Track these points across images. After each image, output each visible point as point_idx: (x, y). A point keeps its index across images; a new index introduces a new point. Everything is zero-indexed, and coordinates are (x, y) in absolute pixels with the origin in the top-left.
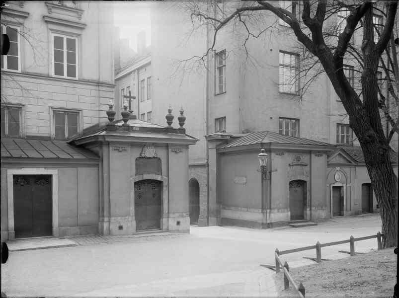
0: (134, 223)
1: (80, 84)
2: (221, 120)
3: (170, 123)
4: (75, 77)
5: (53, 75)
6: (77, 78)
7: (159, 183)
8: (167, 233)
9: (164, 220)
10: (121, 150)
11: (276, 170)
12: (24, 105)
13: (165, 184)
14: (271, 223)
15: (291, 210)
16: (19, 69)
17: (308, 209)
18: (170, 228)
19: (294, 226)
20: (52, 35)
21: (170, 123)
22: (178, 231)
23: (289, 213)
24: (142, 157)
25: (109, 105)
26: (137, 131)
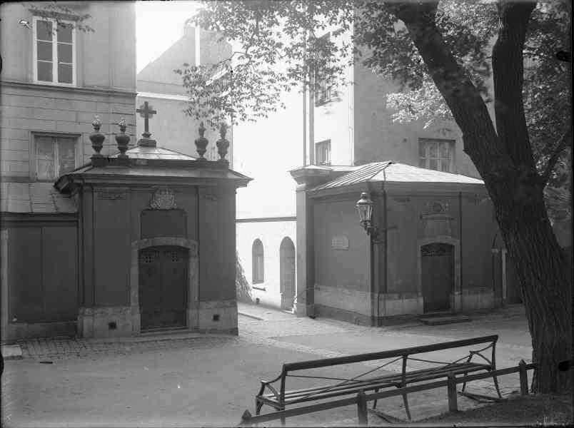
0: (138, 317)
1: (102, 91)
2: (325, 145)
3: (202, 152)
4: (70, 81)
5: (36, 81)
6: (74, 85)
7: (185, 252)
8: (195, 335)
9: (192, 312)
10: (113, 198)
11: (395, 227)
12: (80, 135)
13: (194, 252)
14: (387, 318)
15: (424, 296)
16: (54, 80)
17: (457, 293)
18: (201, 327)
19: (426, 323)
20: (36, 19)
21: (202, 152)
22: (213, 331)
23: (421, 300)
24: (152, 209)
25: (121, 126)
26: (142, 165)
